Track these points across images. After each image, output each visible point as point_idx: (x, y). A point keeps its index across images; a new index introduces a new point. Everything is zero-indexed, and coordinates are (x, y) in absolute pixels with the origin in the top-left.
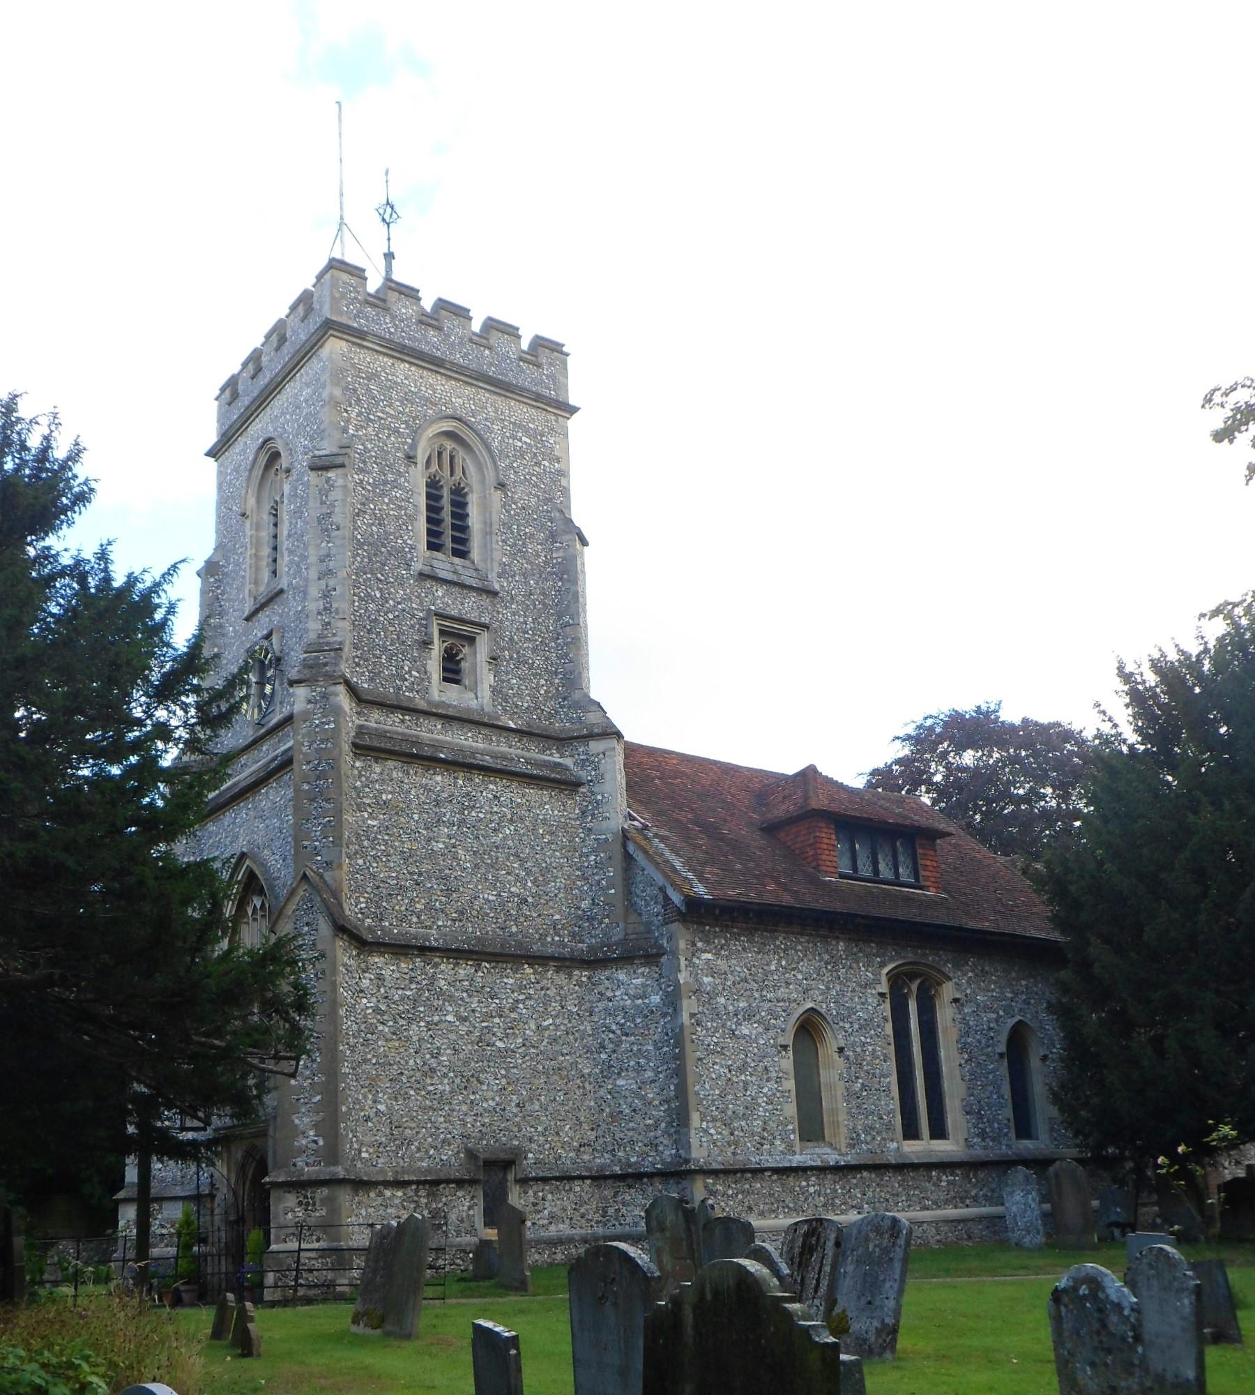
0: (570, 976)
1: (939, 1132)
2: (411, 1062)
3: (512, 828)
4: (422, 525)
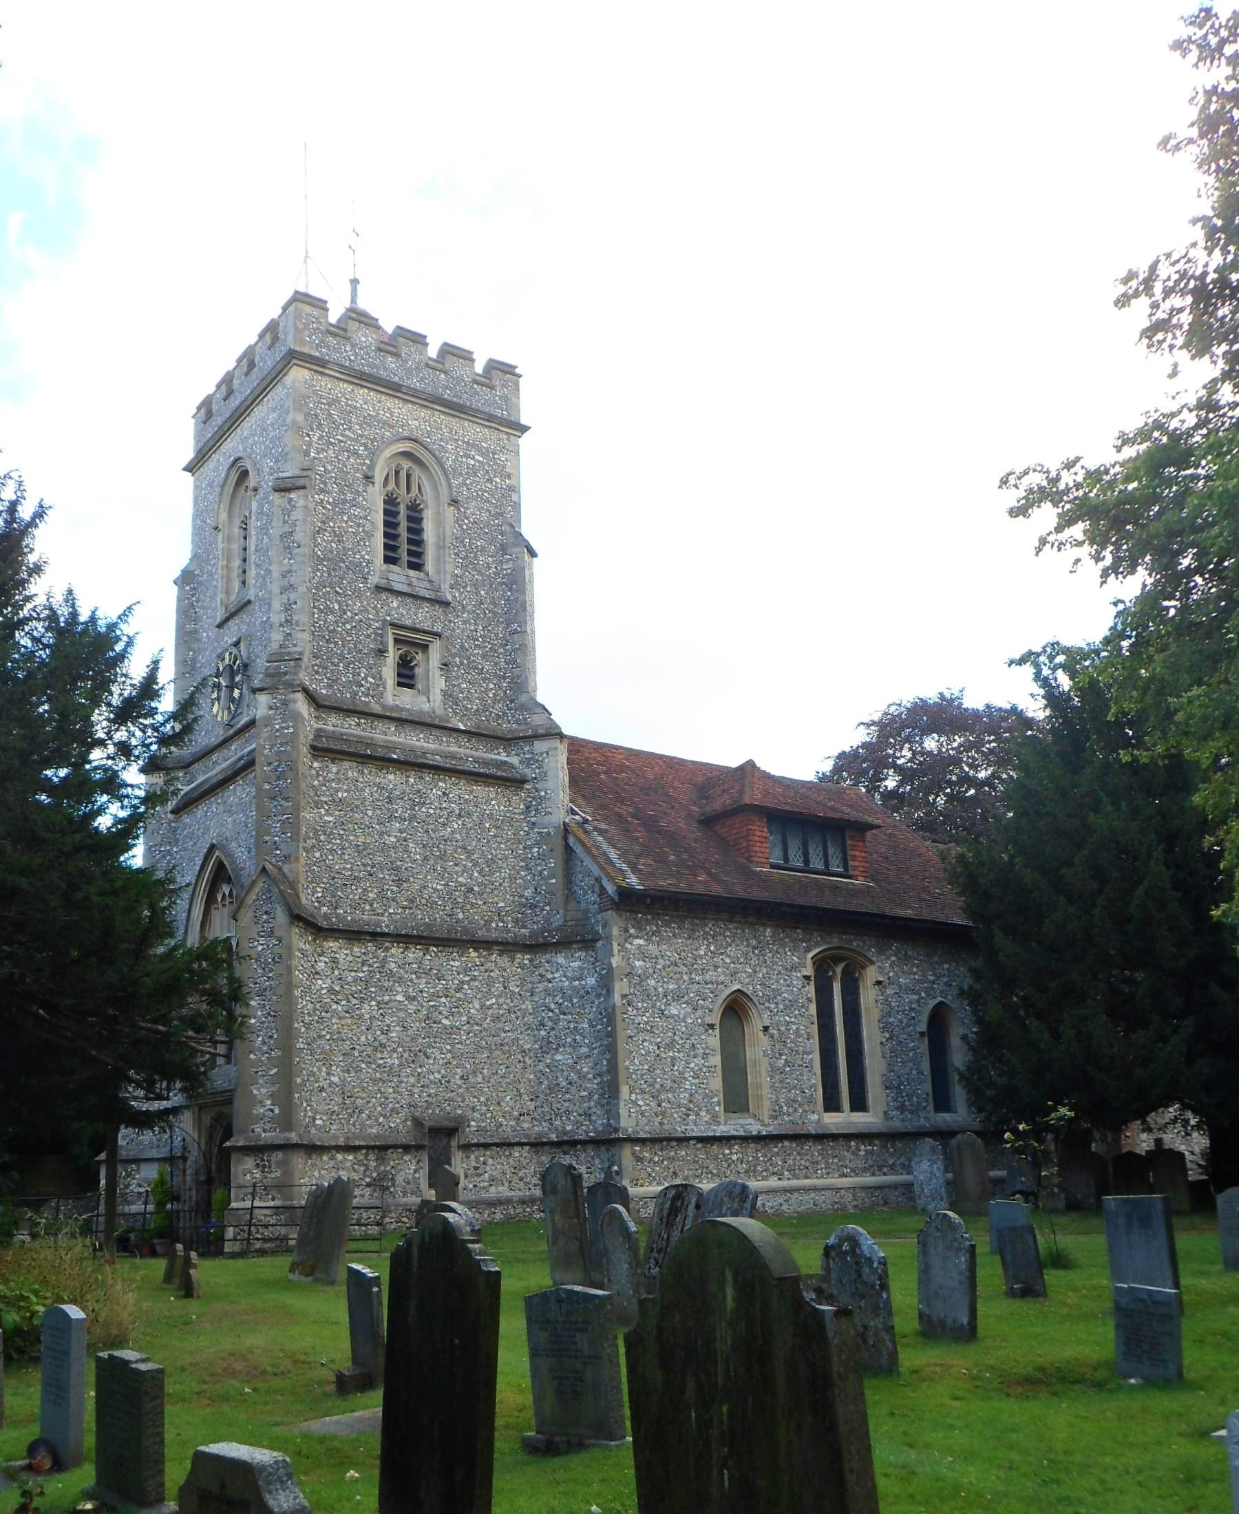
0: (513, 959)
1: (859, 1104)
2: (363, 1038)
3: (460, 822)
4: (379, 540)
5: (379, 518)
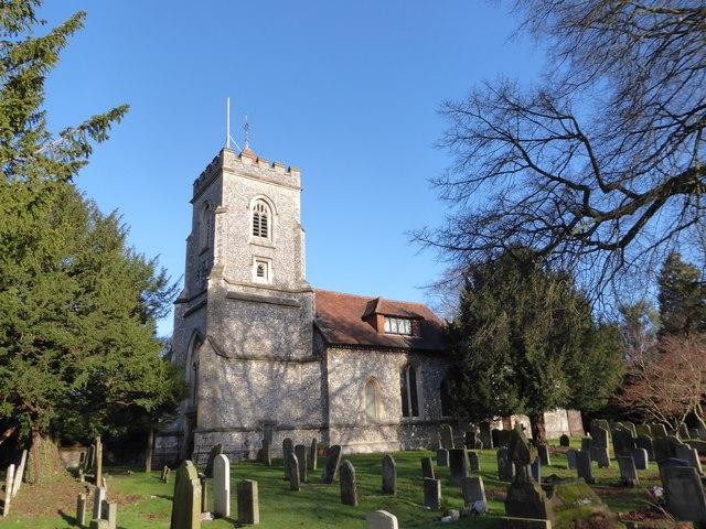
1: (416, 413)
4: (252, 228)
5: (251, 220)
